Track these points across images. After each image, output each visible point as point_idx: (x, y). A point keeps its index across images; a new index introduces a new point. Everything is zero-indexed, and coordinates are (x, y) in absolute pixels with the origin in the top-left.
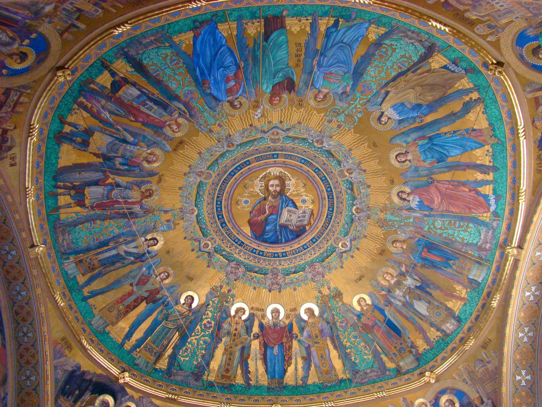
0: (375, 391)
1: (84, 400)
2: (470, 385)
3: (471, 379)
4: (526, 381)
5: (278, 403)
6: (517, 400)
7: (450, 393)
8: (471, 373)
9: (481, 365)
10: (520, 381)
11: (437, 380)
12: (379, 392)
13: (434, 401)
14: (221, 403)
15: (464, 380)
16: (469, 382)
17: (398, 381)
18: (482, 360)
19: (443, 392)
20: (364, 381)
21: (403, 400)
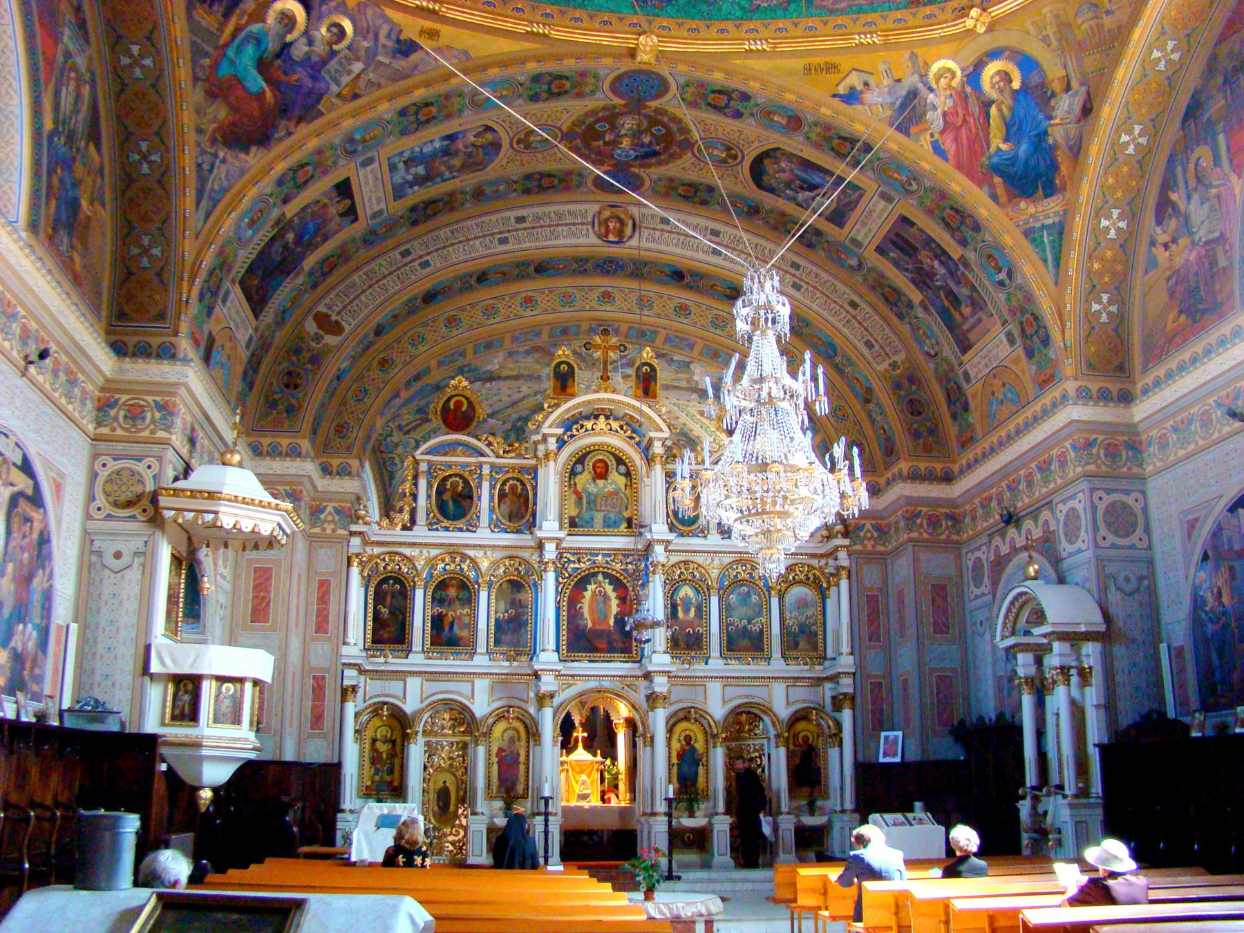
0: (858, 30)
1: (244, 12)
2: (1054, 51)
3: (1060, 40)
4: (1118, 230)
5: (652, 33)
6: (1137, 97)
7: (1009, 58)
8: (1063, 26)
9: (1091, 15)
10: (1107, 229)
11: (991, 29)
12: (865, 34)
13: (971, 69)
14: (532, 23)
15: (1045, 40)
16: (1054, 43)
17: (909, 17)
18: (1096, 6)
19: (994, 54)
20: (838, 6)
21: (911, 58)
